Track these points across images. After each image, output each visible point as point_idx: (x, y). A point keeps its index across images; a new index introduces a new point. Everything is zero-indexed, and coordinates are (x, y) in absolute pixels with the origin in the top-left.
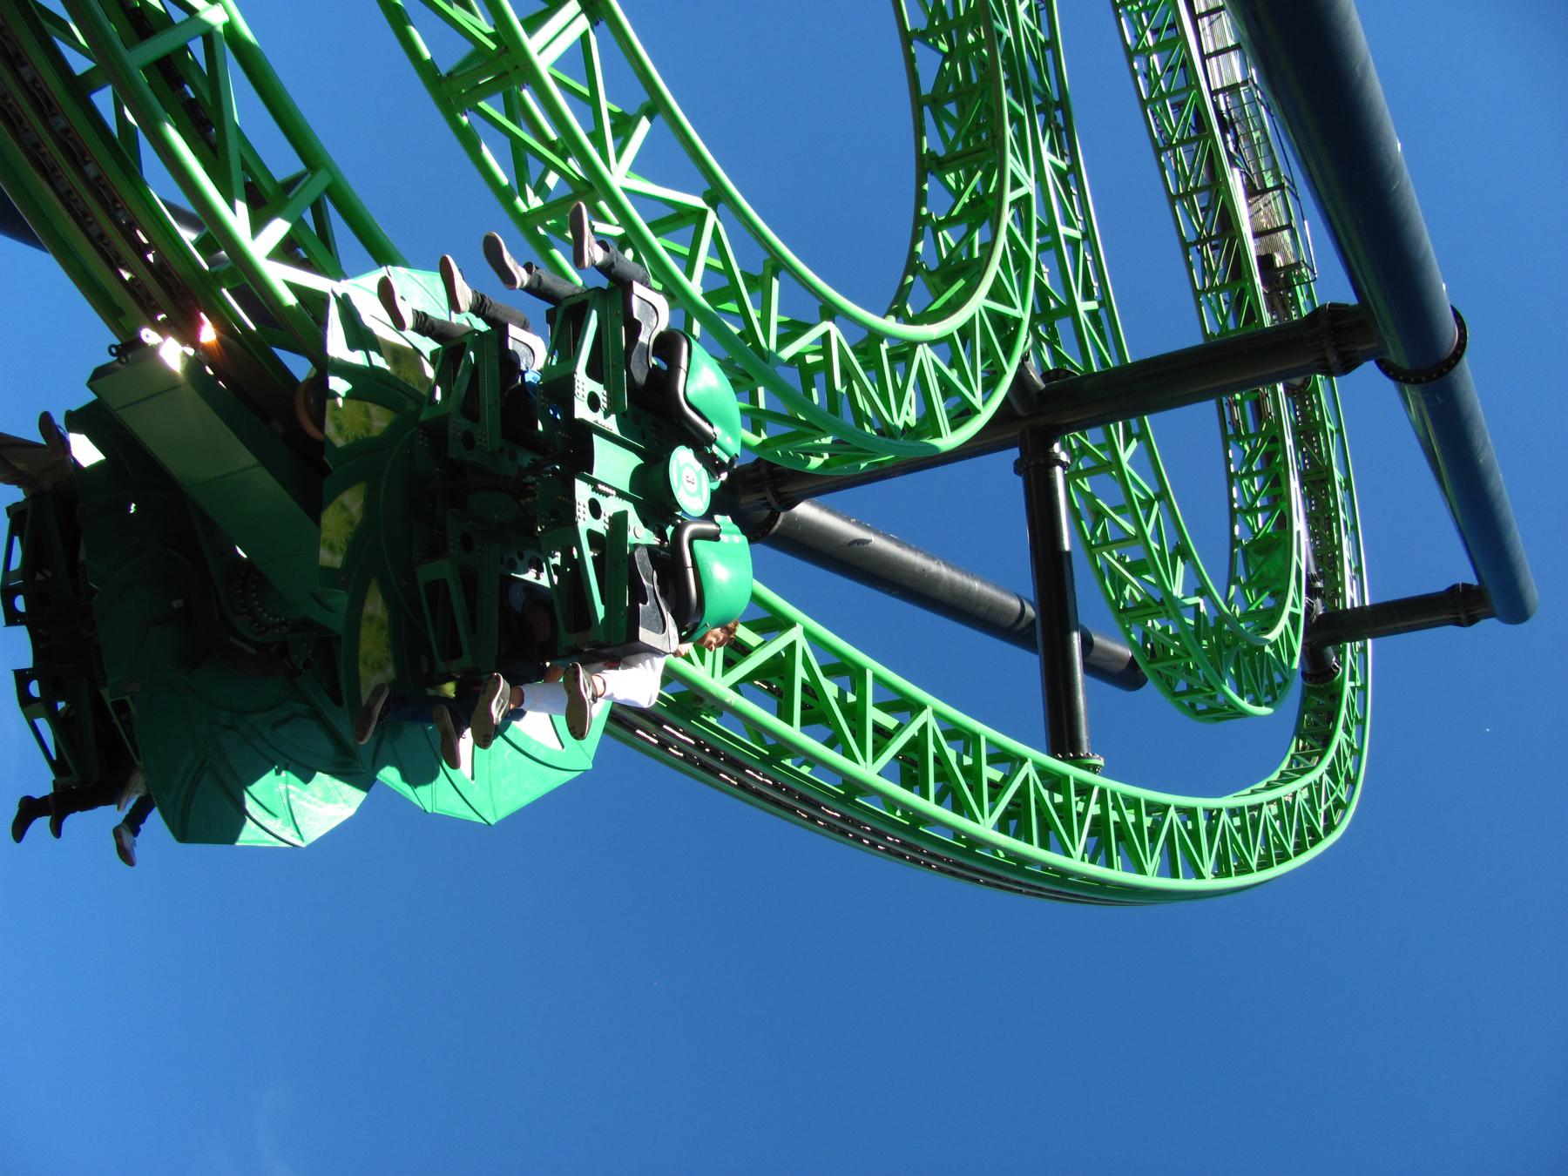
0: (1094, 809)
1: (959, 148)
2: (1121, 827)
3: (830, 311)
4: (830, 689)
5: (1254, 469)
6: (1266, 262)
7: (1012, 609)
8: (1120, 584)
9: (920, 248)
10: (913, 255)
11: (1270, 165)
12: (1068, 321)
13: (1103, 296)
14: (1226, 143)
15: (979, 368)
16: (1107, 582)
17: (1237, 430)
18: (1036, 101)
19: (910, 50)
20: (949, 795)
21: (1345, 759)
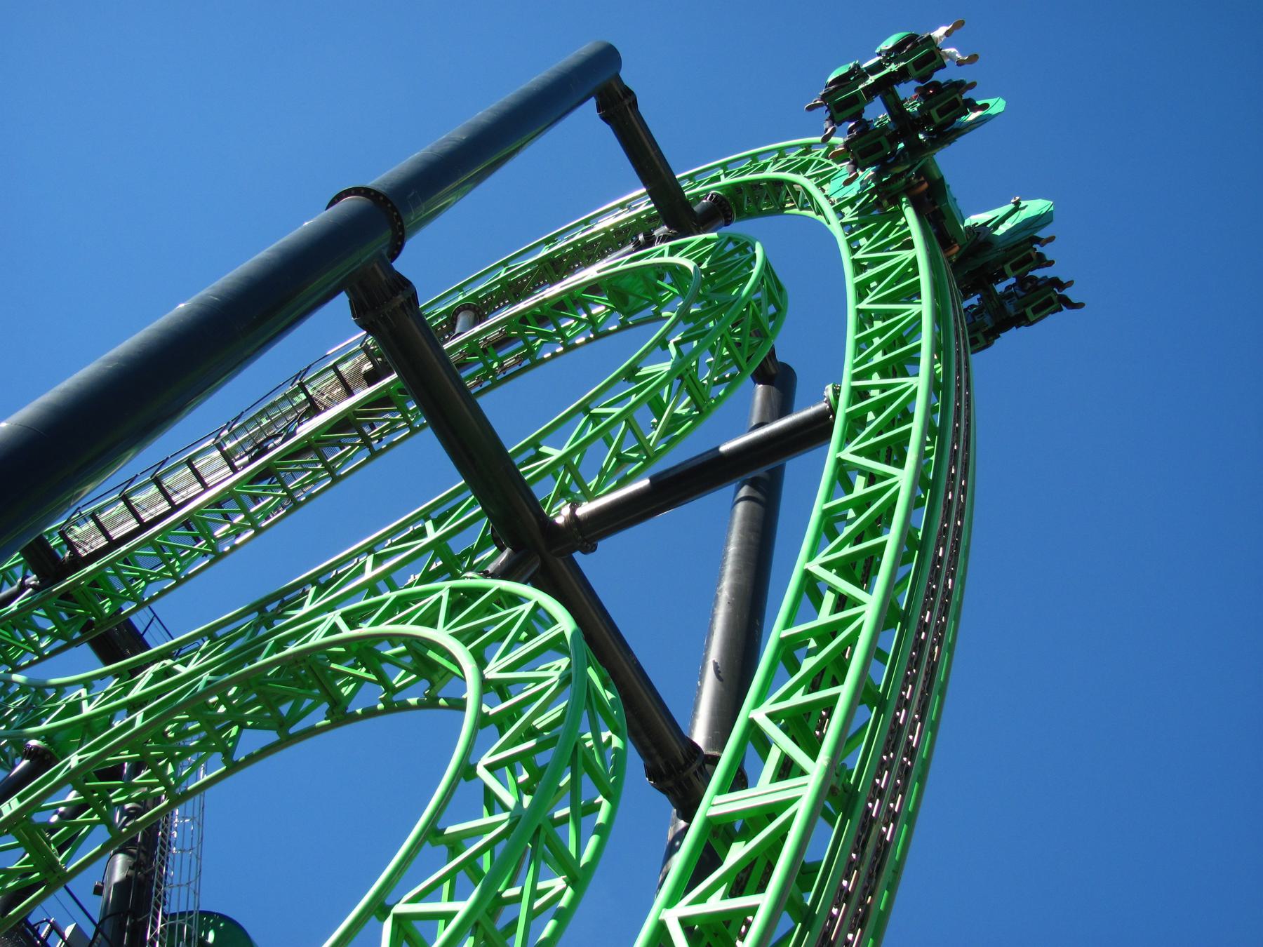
0: (876, 379)
1: (317, 691)
2: (886, 348)
3: (467, 771)
4: (808, 664)
5: (555, 330)
6: (371, 378)
7: (746, 509)
8: (676, 421)
9: (413, 701)
10: (421, 705)
11: (287, 401)
12: (451, 542)
13: (419, 519)
14: (276, 446)
15: (503, 612)
16: (677, 433)
17: (524, 357)
18: (263, 631)
19: (243, 762)
20: (881, 522)
21: (789, 161)
